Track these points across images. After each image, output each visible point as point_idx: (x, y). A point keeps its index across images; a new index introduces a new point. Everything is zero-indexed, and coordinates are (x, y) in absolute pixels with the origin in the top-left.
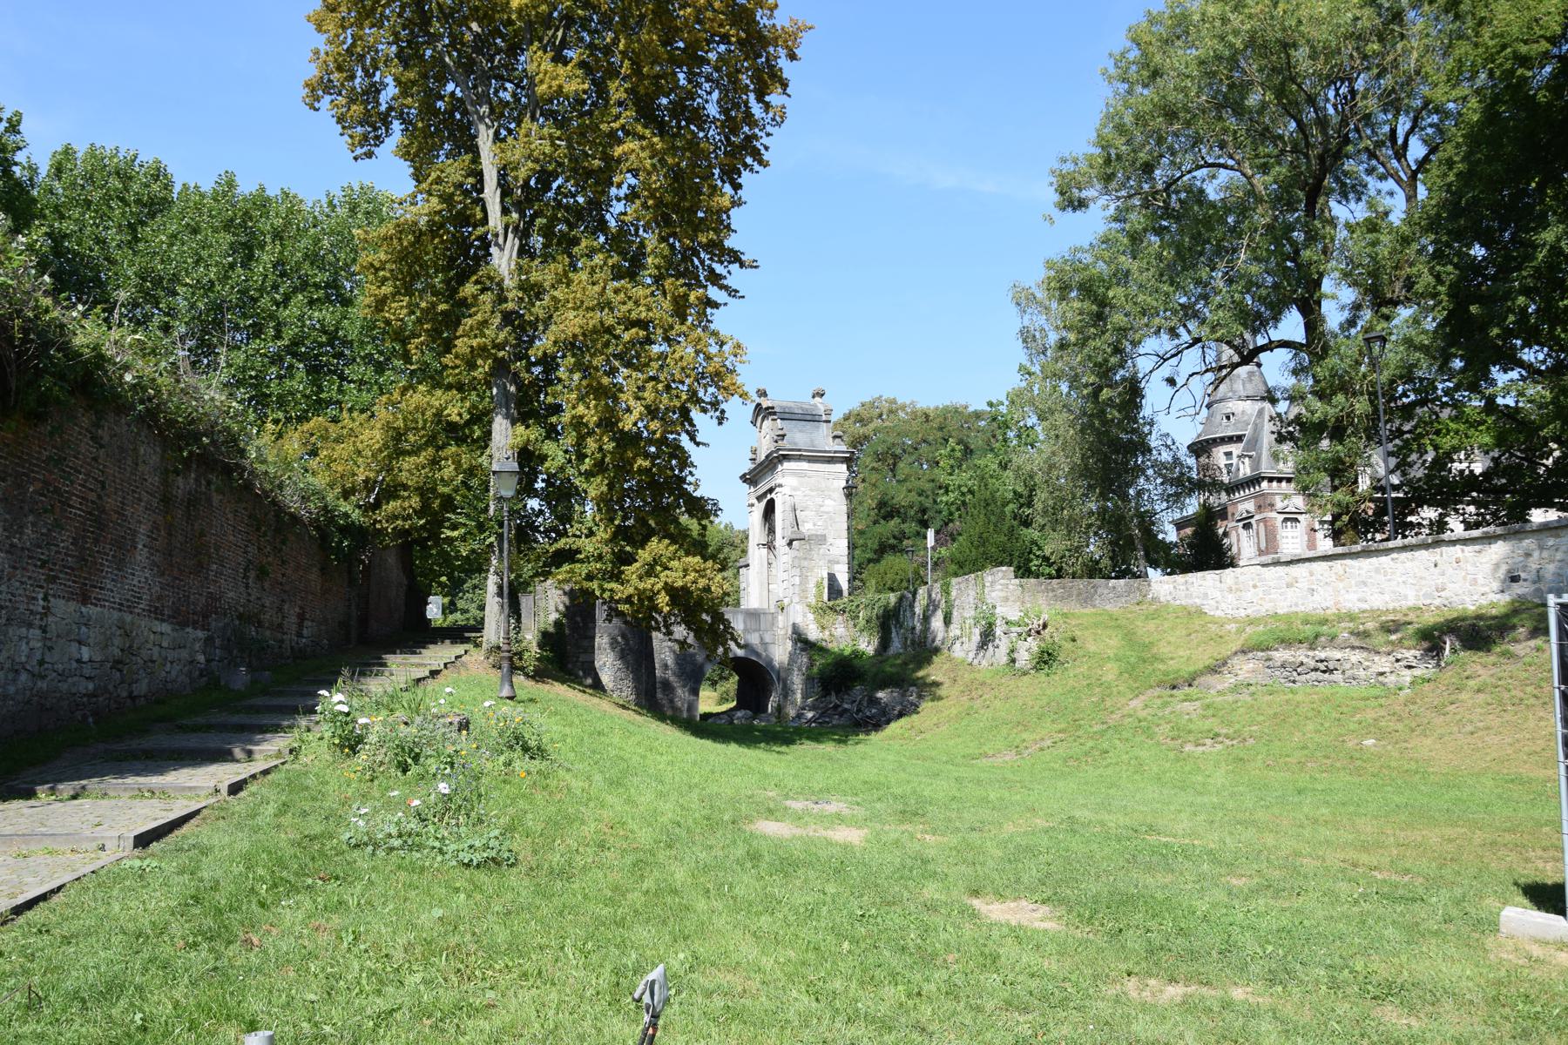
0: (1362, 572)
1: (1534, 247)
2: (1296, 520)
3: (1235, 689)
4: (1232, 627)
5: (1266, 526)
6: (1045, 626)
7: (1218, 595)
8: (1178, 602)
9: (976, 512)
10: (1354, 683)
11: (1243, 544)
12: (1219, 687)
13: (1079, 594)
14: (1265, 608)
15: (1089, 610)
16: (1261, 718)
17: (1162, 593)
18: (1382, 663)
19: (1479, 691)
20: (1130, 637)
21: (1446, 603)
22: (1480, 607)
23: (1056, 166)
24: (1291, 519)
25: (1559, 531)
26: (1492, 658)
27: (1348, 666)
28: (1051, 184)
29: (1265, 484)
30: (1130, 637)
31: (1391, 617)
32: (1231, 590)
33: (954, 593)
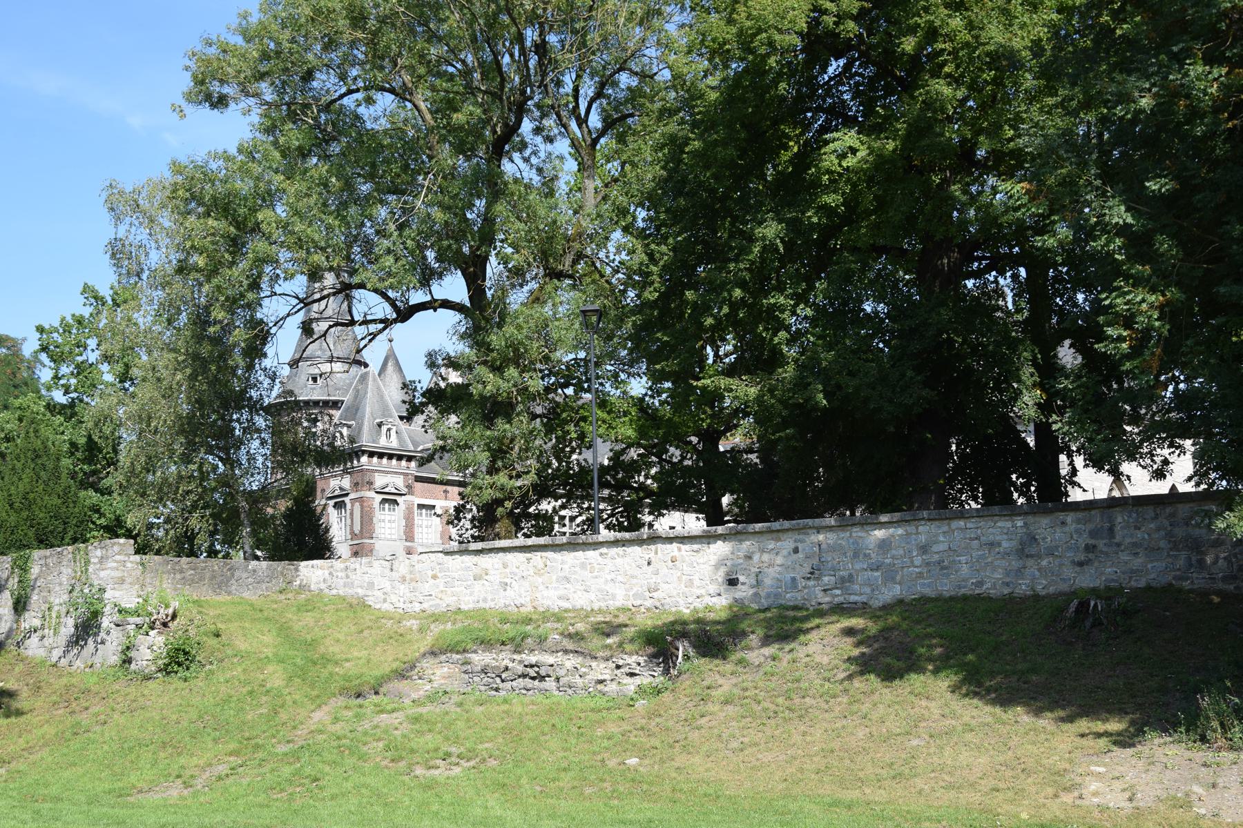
0: (566, 567)
1: (751, 239)
2: (395, 502)
3: (431, 698)
4: (413, 624)
5: (362, 507)
6: (174, 616)
7: (387, 585)
8: (334, 592)
9: (19, 465)
10: (570, 692)
11: (337, 527)
12: (414, 696)
13: (212, 578)
14: (447, 601)
15: (223, 598)
16: (489, 733)
17: (314, 580)
18: (601, 670)
19: (726, 702)
20: (284, 630)
21: (658, 604)
22: (696, 610)
23: (199, 47)
24: (390, 500)
25: (780, 535)
26: (728, 667)
27: (562, 672)
28: (187, 68)
29: (364, 459)
30: (284, 630)
31: (600, 618)
32: (403, 579)
33: (35, 570)
